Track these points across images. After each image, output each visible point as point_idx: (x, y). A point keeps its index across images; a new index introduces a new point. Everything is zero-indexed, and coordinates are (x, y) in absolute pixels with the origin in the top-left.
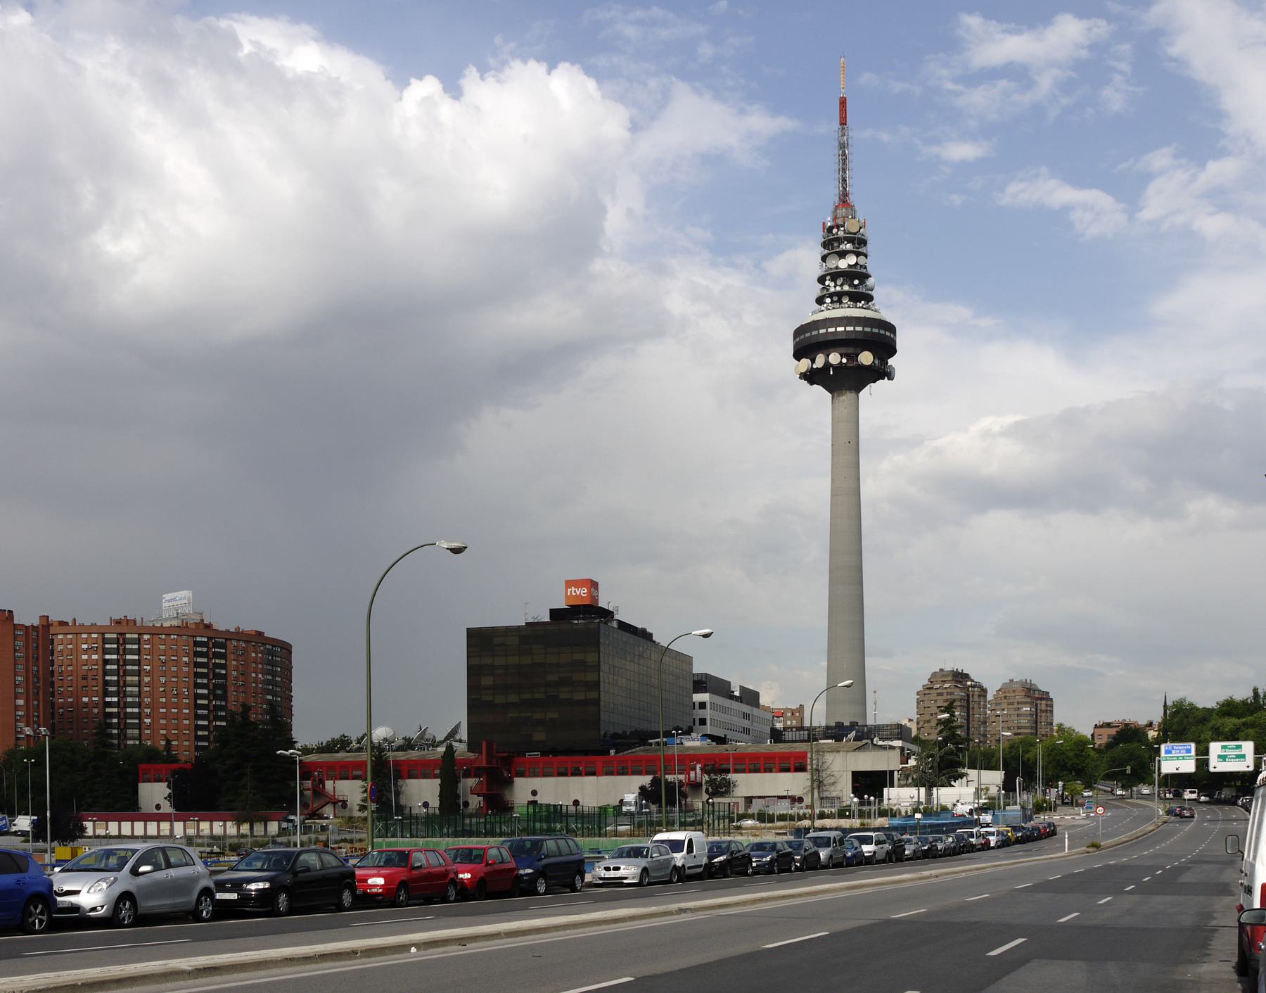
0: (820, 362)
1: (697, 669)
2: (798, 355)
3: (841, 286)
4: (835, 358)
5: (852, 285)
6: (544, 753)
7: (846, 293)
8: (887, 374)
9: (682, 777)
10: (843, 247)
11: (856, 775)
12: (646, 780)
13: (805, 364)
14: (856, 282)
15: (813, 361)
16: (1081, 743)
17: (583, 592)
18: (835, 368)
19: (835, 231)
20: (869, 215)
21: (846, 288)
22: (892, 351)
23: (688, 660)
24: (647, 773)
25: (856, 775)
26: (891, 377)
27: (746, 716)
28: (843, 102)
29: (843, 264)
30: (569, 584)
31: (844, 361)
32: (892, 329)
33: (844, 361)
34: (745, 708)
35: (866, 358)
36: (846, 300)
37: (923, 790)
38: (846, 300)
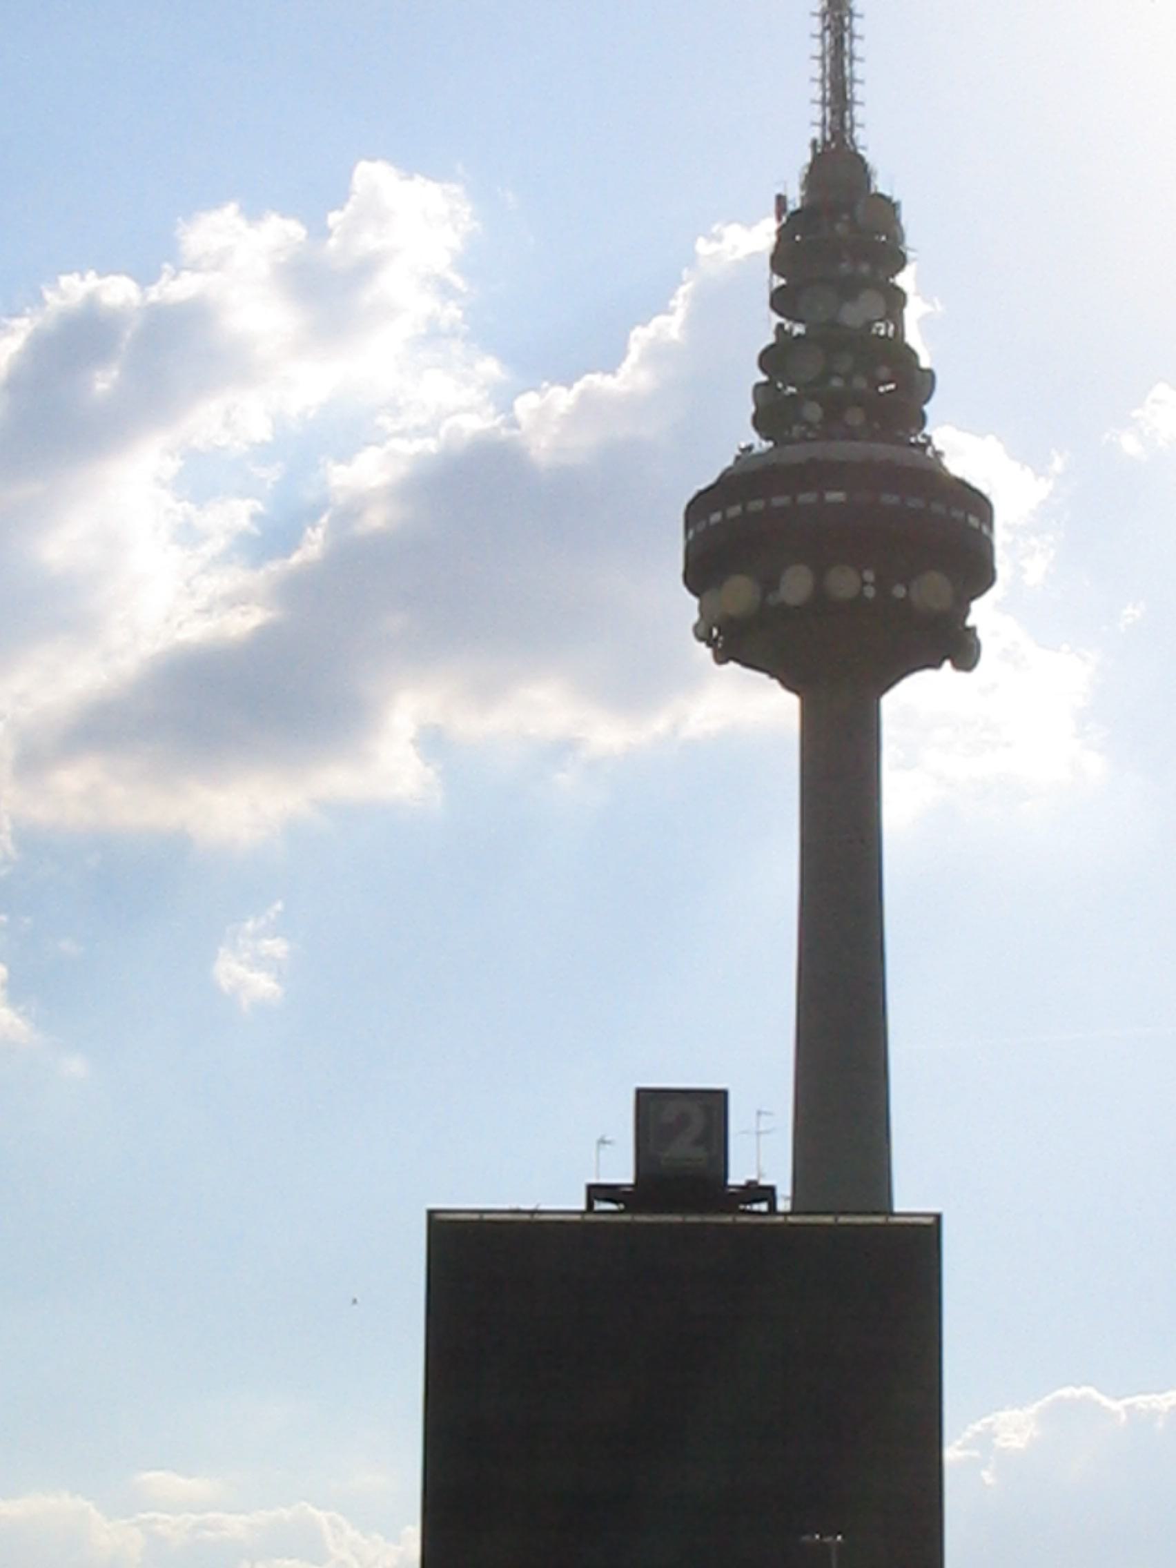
2: (698, 575)
3: (848, 378)
8: (961, 649)
10: (845, 267)
20: (893, 162)
21: (860, 383)
38: (855, 417)
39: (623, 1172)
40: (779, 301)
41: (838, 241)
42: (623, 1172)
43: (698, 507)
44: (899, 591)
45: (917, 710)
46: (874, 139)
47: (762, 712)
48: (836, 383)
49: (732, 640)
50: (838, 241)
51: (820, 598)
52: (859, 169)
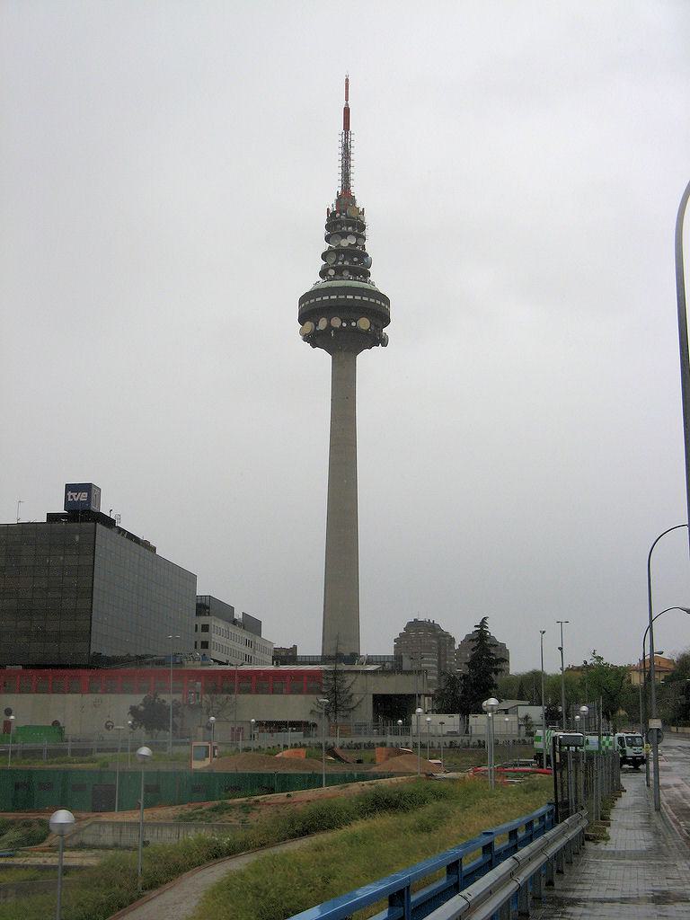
0: (323, 324)
1: (202, 590)
2: (302, 320)
3: (343, 262)
4: (336, 322)
5: (351, 262)
6: (26, 667)
7: (346, 268)
8: (383, 341)
9: (178, 697)
10: (344, 229)
11: (377, 698)
12: (137, 700)
13: (309, 326)
14: (356, 259)
15: (316, 325)
16: (621, 673)
17: (83, 496)
18: (336, 330)
19: (338, 215)
20: (363, 197)
21: (347, 263)
22: (386, 321)
23: (191, 579)
24: (139, 691)
25: (377, 698)
26: (385, 344)
27: (248, 643)
28: (347, 80)
29: (345, 243)
30: (69, 488)
31: (344, 325)
32: (386, 300)
33: (344, 325)
34: (246, 635)
35: (364, 323)
36: (346, 273)
37: (457, 717)
38: (346, 273)
39: (60, 508)
40: (327, 239)
41: (345, 223)
42: (60, 508)
43: (303, 300)
44: (354, 324)
45: (367, 360)
46: (355, 191)
47: (322, 360)
48: (340, 263)
49: (313, 339)
50: (345, 223)
51: (329, 327)
52: (353, 199)
